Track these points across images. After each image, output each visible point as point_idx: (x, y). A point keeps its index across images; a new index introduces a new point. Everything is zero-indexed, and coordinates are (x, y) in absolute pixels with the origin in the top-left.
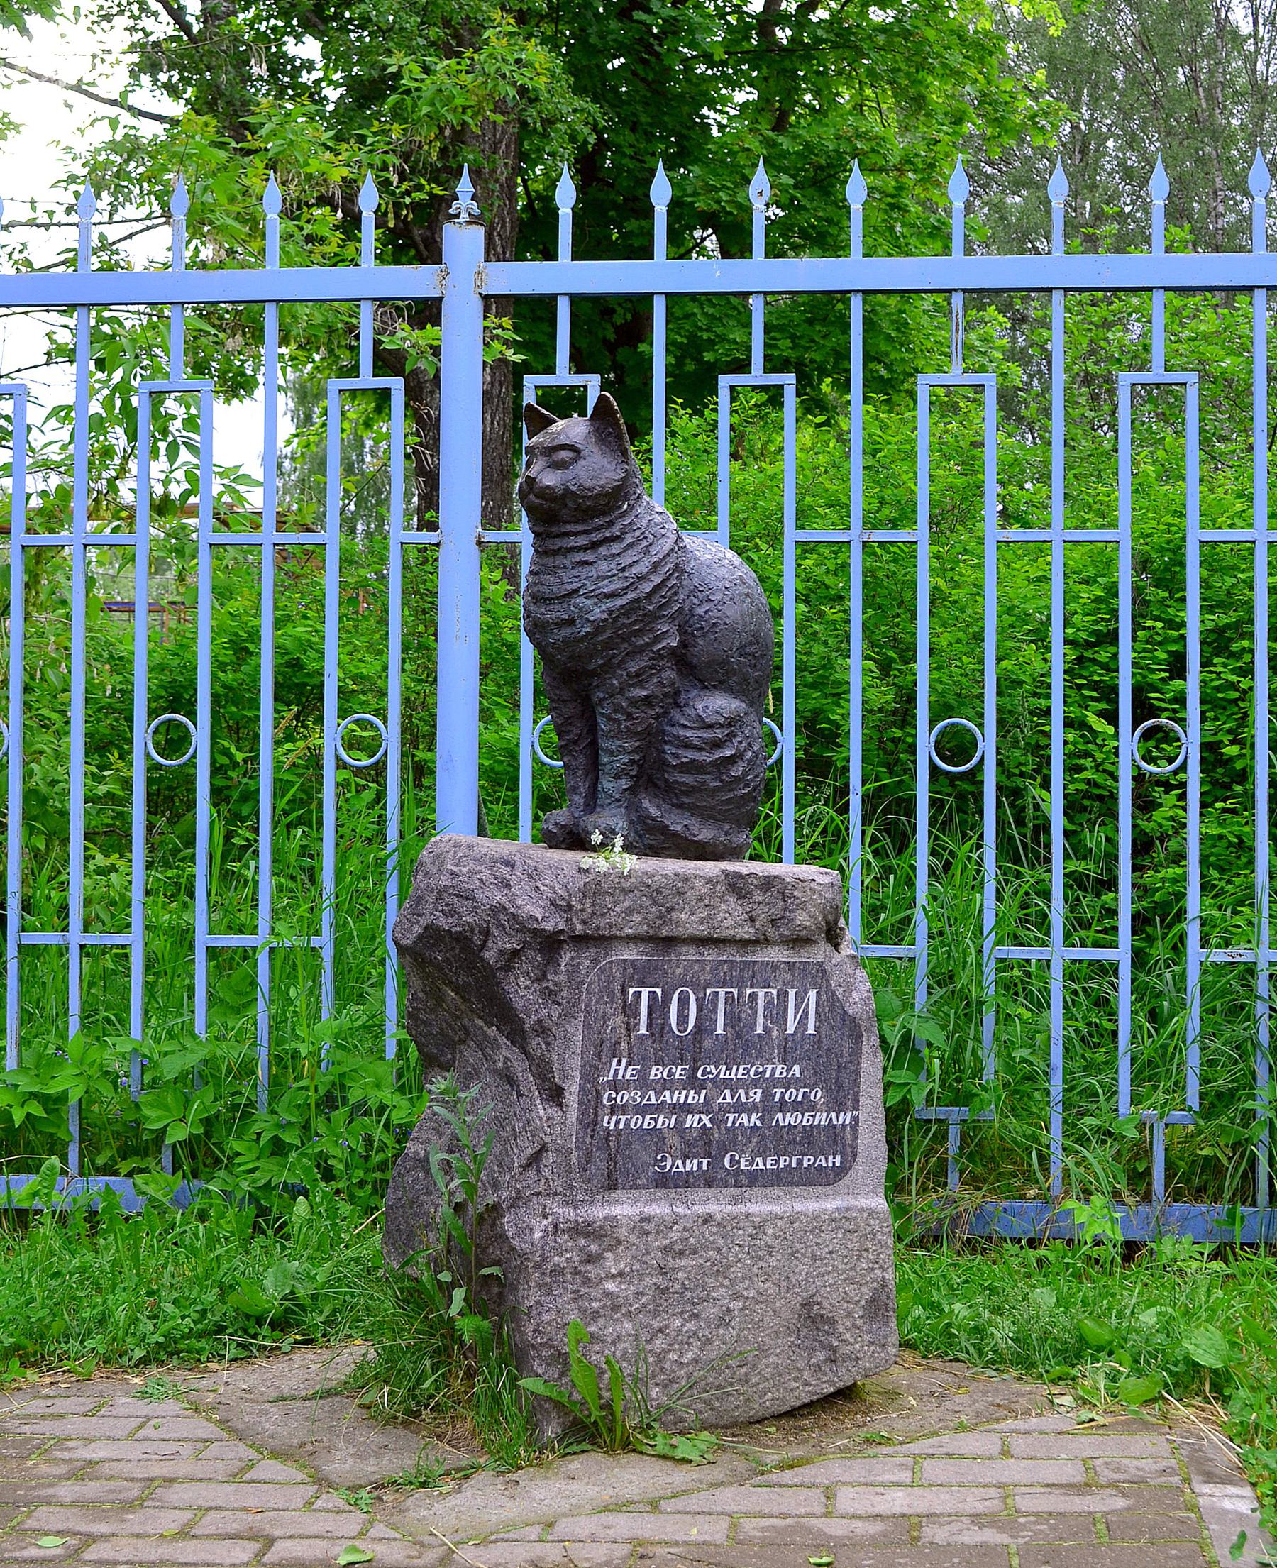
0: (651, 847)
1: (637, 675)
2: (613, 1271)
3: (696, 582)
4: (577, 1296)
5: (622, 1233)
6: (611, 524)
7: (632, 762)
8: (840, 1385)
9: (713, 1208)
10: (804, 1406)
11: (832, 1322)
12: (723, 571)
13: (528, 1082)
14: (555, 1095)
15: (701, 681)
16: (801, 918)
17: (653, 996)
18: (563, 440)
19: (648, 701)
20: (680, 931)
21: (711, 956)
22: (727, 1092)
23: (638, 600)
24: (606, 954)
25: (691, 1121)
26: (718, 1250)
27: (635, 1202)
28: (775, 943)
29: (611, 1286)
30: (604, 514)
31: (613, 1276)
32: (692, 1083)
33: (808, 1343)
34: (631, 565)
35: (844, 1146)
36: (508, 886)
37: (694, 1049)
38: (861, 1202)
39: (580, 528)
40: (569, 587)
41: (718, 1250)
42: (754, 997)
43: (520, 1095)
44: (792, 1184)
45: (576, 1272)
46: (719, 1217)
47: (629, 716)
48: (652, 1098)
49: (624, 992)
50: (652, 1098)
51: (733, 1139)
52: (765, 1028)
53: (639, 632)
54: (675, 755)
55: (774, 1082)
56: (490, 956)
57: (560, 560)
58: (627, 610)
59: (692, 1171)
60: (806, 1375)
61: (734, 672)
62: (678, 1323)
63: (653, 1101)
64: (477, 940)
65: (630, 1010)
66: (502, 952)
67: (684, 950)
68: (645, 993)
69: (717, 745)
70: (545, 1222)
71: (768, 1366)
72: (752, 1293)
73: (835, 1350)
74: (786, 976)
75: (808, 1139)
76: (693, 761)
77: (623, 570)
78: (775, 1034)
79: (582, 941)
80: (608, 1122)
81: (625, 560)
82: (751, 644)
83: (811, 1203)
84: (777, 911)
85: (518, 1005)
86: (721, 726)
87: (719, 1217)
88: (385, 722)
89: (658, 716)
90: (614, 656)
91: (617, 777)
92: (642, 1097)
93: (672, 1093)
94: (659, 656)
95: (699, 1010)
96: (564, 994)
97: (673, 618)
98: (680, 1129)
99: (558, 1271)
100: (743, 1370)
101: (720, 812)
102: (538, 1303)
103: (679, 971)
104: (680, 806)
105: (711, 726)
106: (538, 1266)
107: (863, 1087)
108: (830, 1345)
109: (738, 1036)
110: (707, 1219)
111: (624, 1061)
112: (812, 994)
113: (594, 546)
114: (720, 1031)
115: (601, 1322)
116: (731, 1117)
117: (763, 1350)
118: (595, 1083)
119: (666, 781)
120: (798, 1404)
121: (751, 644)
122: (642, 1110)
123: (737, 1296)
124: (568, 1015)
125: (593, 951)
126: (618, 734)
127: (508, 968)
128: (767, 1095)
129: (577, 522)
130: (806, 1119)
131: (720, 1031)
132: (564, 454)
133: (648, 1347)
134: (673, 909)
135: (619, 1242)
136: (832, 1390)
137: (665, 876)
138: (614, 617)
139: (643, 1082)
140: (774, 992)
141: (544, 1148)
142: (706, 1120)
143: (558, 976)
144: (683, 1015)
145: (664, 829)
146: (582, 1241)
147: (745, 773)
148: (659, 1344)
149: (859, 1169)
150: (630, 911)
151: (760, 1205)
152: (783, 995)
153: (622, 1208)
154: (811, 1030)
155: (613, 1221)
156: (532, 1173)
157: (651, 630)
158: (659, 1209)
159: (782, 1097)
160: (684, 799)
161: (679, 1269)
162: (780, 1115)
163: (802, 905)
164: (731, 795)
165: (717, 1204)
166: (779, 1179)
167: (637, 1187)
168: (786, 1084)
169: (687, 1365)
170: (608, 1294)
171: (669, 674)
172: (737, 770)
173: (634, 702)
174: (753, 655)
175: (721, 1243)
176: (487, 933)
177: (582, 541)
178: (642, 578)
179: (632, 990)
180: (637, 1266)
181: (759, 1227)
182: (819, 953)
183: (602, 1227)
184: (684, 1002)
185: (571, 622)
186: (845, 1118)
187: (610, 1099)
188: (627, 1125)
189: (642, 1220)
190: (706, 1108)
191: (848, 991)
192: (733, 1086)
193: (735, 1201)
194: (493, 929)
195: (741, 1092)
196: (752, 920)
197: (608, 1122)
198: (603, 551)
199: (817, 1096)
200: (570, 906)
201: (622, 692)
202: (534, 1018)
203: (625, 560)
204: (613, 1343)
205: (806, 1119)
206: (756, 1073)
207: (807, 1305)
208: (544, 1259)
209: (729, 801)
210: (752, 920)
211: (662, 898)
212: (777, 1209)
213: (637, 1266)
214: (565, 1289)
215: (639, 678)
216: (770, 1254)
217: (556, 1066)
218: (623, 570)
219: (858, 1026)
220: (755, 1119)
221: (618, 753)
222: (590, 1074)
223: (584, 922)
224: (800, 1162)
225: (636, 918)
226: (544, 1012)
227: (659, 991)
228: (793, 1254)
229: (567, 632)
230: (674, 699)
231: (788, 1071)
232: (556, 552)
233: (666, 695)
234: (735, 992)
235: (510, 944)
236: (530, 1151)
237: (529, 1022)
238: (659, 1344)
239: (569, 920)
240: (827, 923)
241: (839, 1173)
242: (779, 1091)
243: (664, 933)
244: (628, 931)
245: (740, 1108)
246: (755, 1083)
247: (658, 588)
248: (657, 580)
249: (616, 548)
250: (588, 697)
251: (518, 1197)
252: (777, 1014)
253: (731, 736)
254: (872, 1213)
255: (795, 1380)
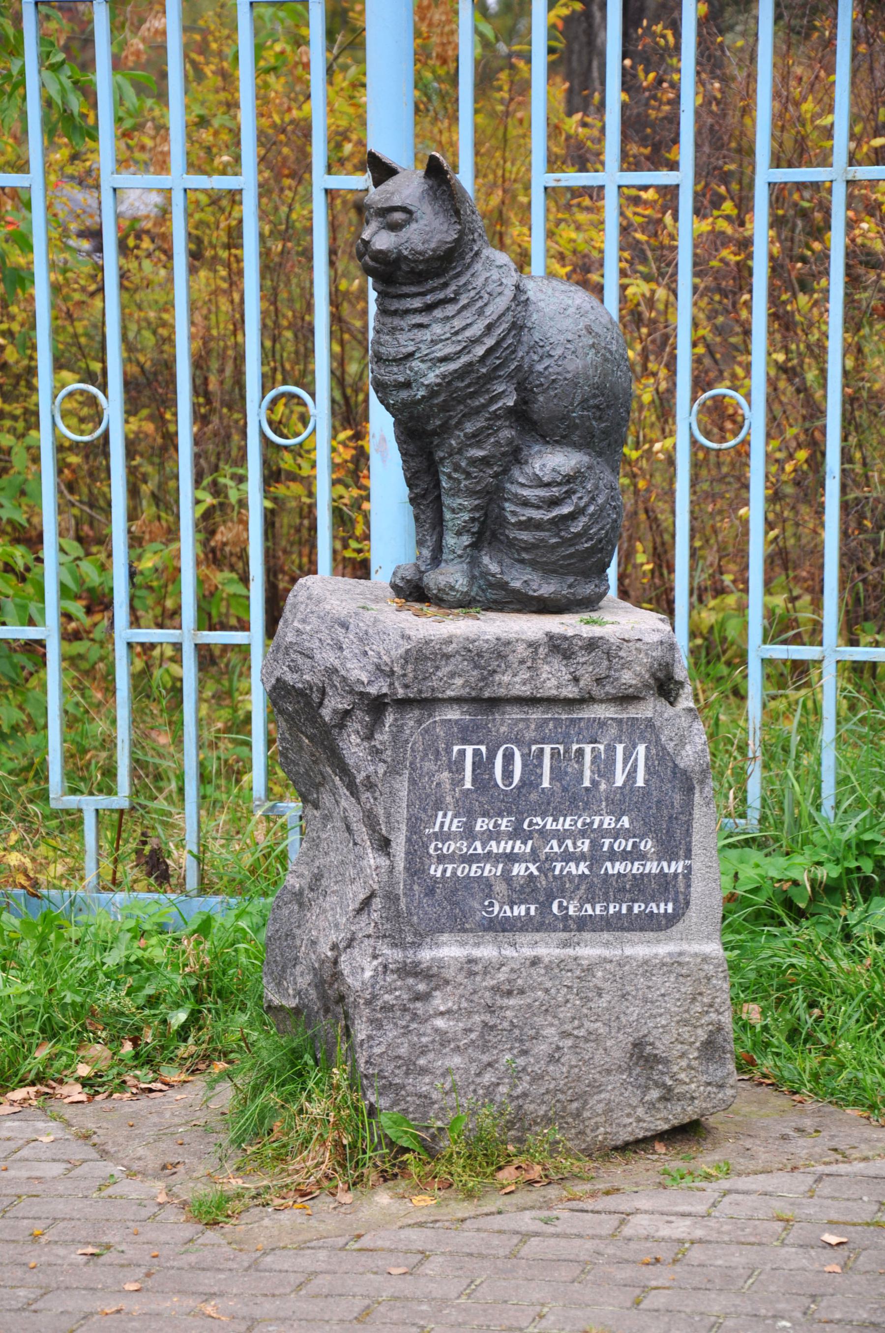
0: (495, 602)
1: (474, 435)
2: (442, 1008)
3: (537, 336)
4: (406, 1032)
5: (449, 974)
6: (446, 285)
7: (473, 520)
8: (676, 1122)
9: (542, 951)
10: (638, 1142)
11: (666, 1062)
12: (568, 323)
13: (362, 832)
14: (384, 845)
15: (543, 437)
16: (627, 677)
17: (477, 753)
18: (397, 201)
19: (485, 461)
20: (502, 692)
21: (536, 715)
22: (554, 843)
23: (471, 364)
24: (430, 716)
25: (518, 869)
26: (547, 991)
27: (463, 944)
28: (602, 701)
29: (440, 1023)
30: (438, 275)
31: (442, 1014)
32: (517, 833)
33: (642, 1081)
34: (464, 328)
35: (677, 893)
36: (341, 648)
37: (521, 802)
38: (695, 948)
39: (414, 289)
40: (405, 350)
41: (547, 991)
42: (580, 752)
43: (355, 844)
44: (623, 929)
45: (405, 1009)
46: (546, 960)
47: (468, 475)
48: (471, 848)
49: (448, 750)
50: (471, 848)
51: (561, 887)
52: (593, 782)
53: (472, 395)
54: (514, 513)
55: (603, 833)
56: (326, 713)
57: (397, 321)
58: (460, 374)
59: (519, 917)
60: (640, 1112)
61: (576, 427)
62: (508, 1057)
63: (480, 851)
64: (316, 697)
65: (457, 767)
66: (335, 711)
67: (508, 709)
68: (469, 750)
69: (554, 502)
70: (375, 963)
71: (599, 1102)
72: (582, 1033)
73: (669, 1089)
74: (613, 731)
75: (638, 888)
76: (530, 519)
77: (456, 333)
78: (603, 787)
79: (404, 704)
80: (435, 870)
81: (458, 323)
82: (595, 396)
83: (641, 948)
84: (602, 671)
85: (351, 762)
86: (559, 484)
87: (546, 960)
88: (54, 424)
89: (496, 475)
90: (451, 417)
91: (459, 534)
92: (469, 848)
93: (498, 843)
94: (495, 416)
95: (524, 765)
96: (389, 752)
97: (510, 377)
98: (506, 877)
99: (387, 1008)
100: (575, 1105)
101: (561, 566)
102: (370, 1037)
103: (503, 729)
104: (522, 561)
105: (548, 485)
106: (368, 1003)
107: (695, 838)
108: (664, 1085)
109: (565, 789)
110: (535, 962)
111: (450, 814)
112: (641, 749)
113: (429, 308)
114: (546, 784)
115: (431, 1056)
116: (559, 866)
117: (597, 1088)
118: (420, 833)
119: (507, 537)
120: (631, 1139)
121: (595, 396)
122: (470, 859)
123: (565, 1035)
124: (393, 771)
125: (417, 713)
126: (456, 492)
127: (341, 726)
128: (595, 845)
129: (412, 284)
130: (636, 868)
131: (546, 784)
132: (398, 216)
133: (478, 1080)
134: (495, 671)
135: (447, 982)
136: (666, 1127)
137: (487, 641)
138: (449, 380)
139: (469, 834)
140: (602, 747)
141: (372, 895)
142: (533, 869)
143: (383, 737)
144: (509, 770)
145: (503, 586)
146: (411, 981)
147: (587, 528)
148: (488, 1078)
149: (693, 915)
150: (452, 675)
151: (591, 949)
152: (611, 749)
153: (449, 951)
154: (640, 783)
155: (441, 963)
156: (364, 917)
157: (488, 391)
158: (487, 952)
159: (611, 846)
160: (525, 556)
161: (508, 1008)
162: (608, 864)
163: (627, 665)
164: (572, 550)
165: (547, 948)
166: (608, 924)
167: (465, 931)
168: (616, 834)
169: (518, 1097)
170: (437, 1030)
171: (507, 433)
172: (577, 527)
173: (473, 461)
174: (597, 407)
175: (549, 984)
176: (323, 692)
177: (417, 303)
178: (476, 341)
179: (456, 748)
180: (464, 1004)
181: (589, 970)
182: (647, 710)
183: (429, 968)
184: (508, 758)
185: (407, 385)
186: (678, 867)
187: (436, 849)
188: (454, 873)
189: (470, 961)
190: (534, 856)
191: (682, 743)
192: (561, 837)
193: (565, 944)
194: (328, 689)
195: (569, 842)
196: (576, 680)
197: (435, 870)
198: (438, 313)
199: (648, 845)
200: (392, 672)
201: (460, 452)
202: (363, 774)
203: (458, 323)
204: (443, 1075)
205: (636, 868)
206: (584, 824)
207: (638, 1045)
208: (374, 997)
209: (571, 556)
210: (576, 680)
211: (488, 658)
212: (606, 953)
213: (464, 1004)
214: (395, 1024)
215: (476, 439)
216: (600, 995)
217: (382, 819)
218: (456, 333)
219: (689, 779)
220: (583, 868)
221: (459, 510)
222: (414, 826)
223: (406, 686)
224: (630, 909)
225: (459, 681)
226: (371, 768)
227: (483, 748)
228: (623, 996)
229: (404, 394)
230: (515, 456)
231: (617, 821)
232: (395, 313)
233: (504, 454)
234: (561, 748)
235: (344, 705)
236: (362, 896)
237: (360, 778)
238: (488, 1078)
239: (391, 684)
240: (657, 679)
241: (671, 920)
242: (607, 842)
243: (486, 694)
244: (450, 693)
245: (567, 857)
246: (583, 834)
247: (490, 351)
248: (490, 342)
249: (451, 310)
250: (431, 454)
251: (352, 940)
252: (604, 768)
253: (569, 494)
254: (705, 959)
255: (629, 1115)
